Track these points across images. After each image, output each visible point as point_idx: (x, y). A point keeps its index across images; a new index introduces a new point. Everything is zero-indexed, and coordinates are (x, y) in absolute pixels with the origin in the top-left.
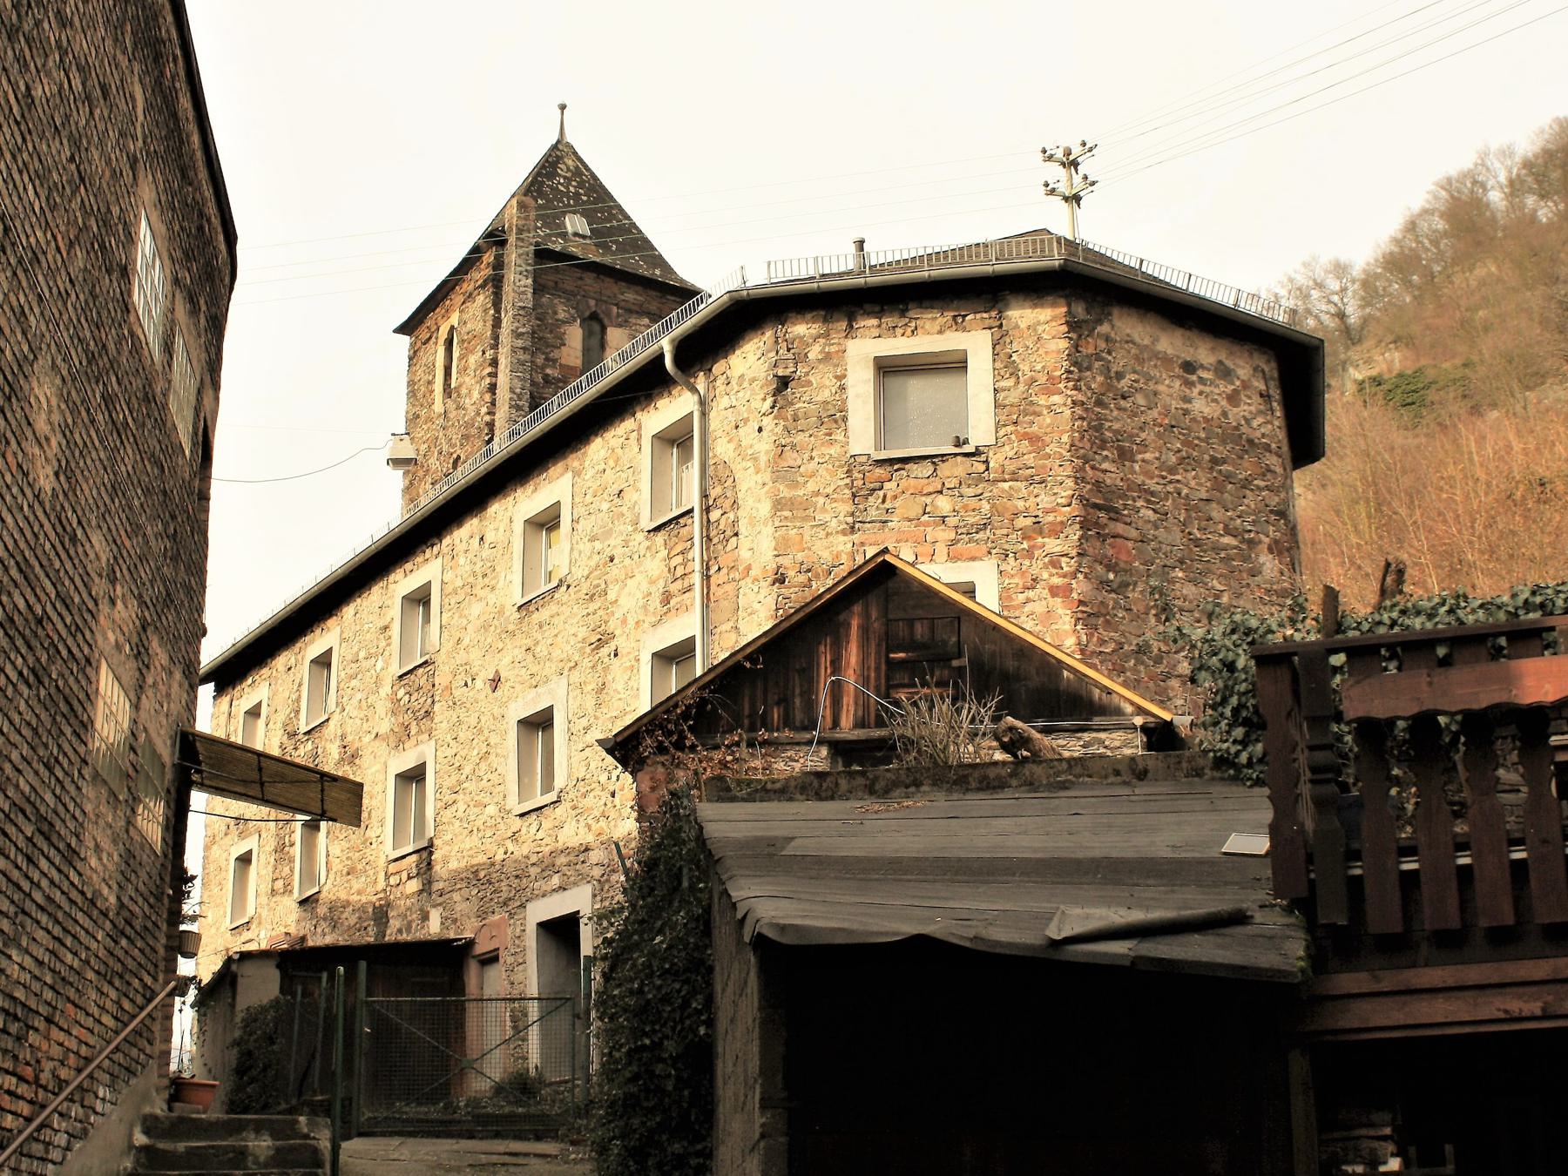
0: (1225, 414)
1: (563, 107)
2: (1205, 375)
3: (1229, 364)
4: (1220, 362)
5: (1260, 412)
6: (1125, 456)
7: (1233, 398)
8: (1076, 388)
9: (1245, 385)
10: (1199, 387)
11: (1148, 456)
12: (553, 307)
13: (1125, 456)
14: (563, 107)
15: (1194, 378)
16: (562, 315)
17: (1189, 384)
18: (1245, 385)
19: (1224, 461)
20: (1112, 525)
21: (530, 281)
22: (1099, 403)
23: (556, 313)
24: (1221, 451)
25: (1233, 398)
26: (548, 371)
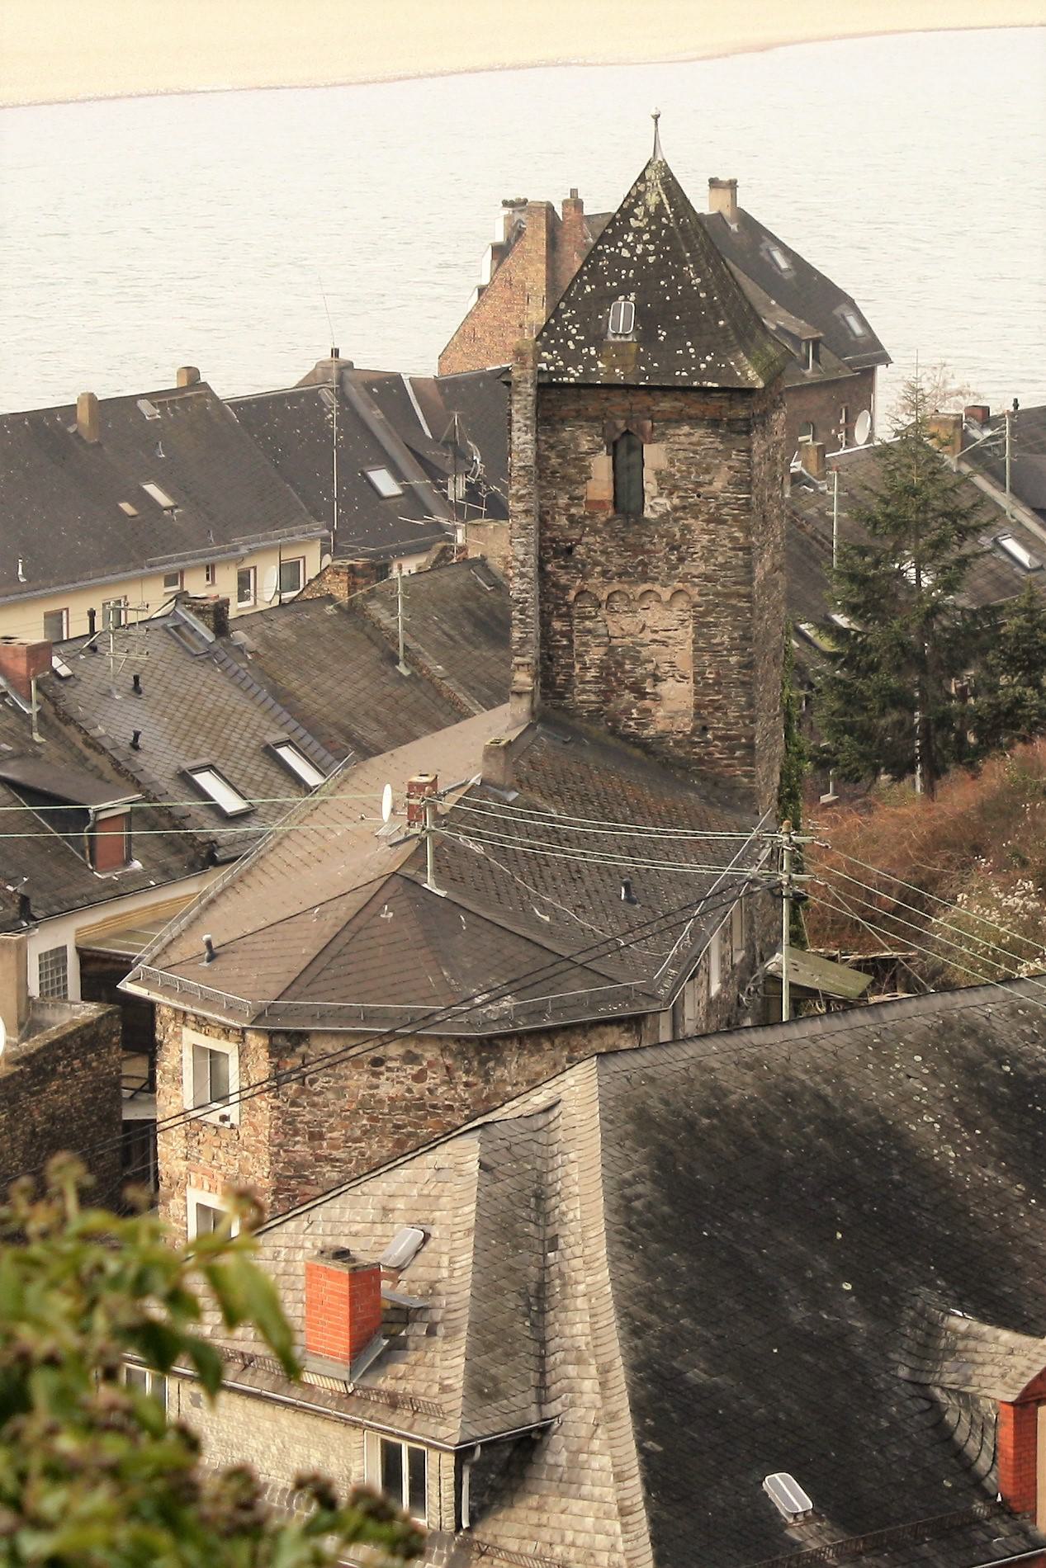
0: (409, 1090)
1: (656, 117)
2: (390, 1064)
3: (418, 1051)
4: (409, 1052)
5: (444, 1083)
6: (316, 1137)
7: (419, 1077)
8: (275, 1097)
9: (430, 1064)
10: (387, 1074)
11: (335, 1134)
12: (574, 439)
13: (316, 1137)
14: (656, 117)
15: (383, 1069)
16: (585, 446)
17: (376, 1075)
18: (430, 1064)
19: (405, 1126)
20: (302, 1187)
21: (529, 437)
22: (294, 1104)
23: (577, 445)
24: (400, 1118)
25: (419, 1077)
26: (573, 511)
